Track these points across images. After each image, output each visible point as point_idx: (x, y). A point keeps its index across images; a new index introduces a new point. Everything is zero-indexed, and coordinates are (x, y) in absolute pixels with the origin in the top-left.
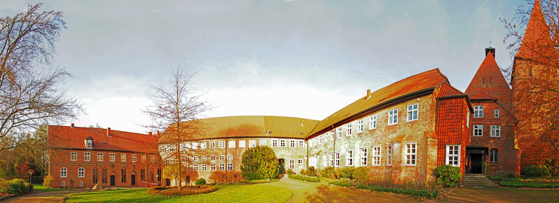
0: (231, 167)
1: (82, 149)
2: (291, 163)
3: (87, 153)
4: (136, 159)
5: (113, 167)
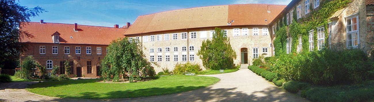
0: (56, 50)
1: (72, 44)
2: (254, 52)
3: (55, 47)
4: (80, 51)
5: (79, 59)
